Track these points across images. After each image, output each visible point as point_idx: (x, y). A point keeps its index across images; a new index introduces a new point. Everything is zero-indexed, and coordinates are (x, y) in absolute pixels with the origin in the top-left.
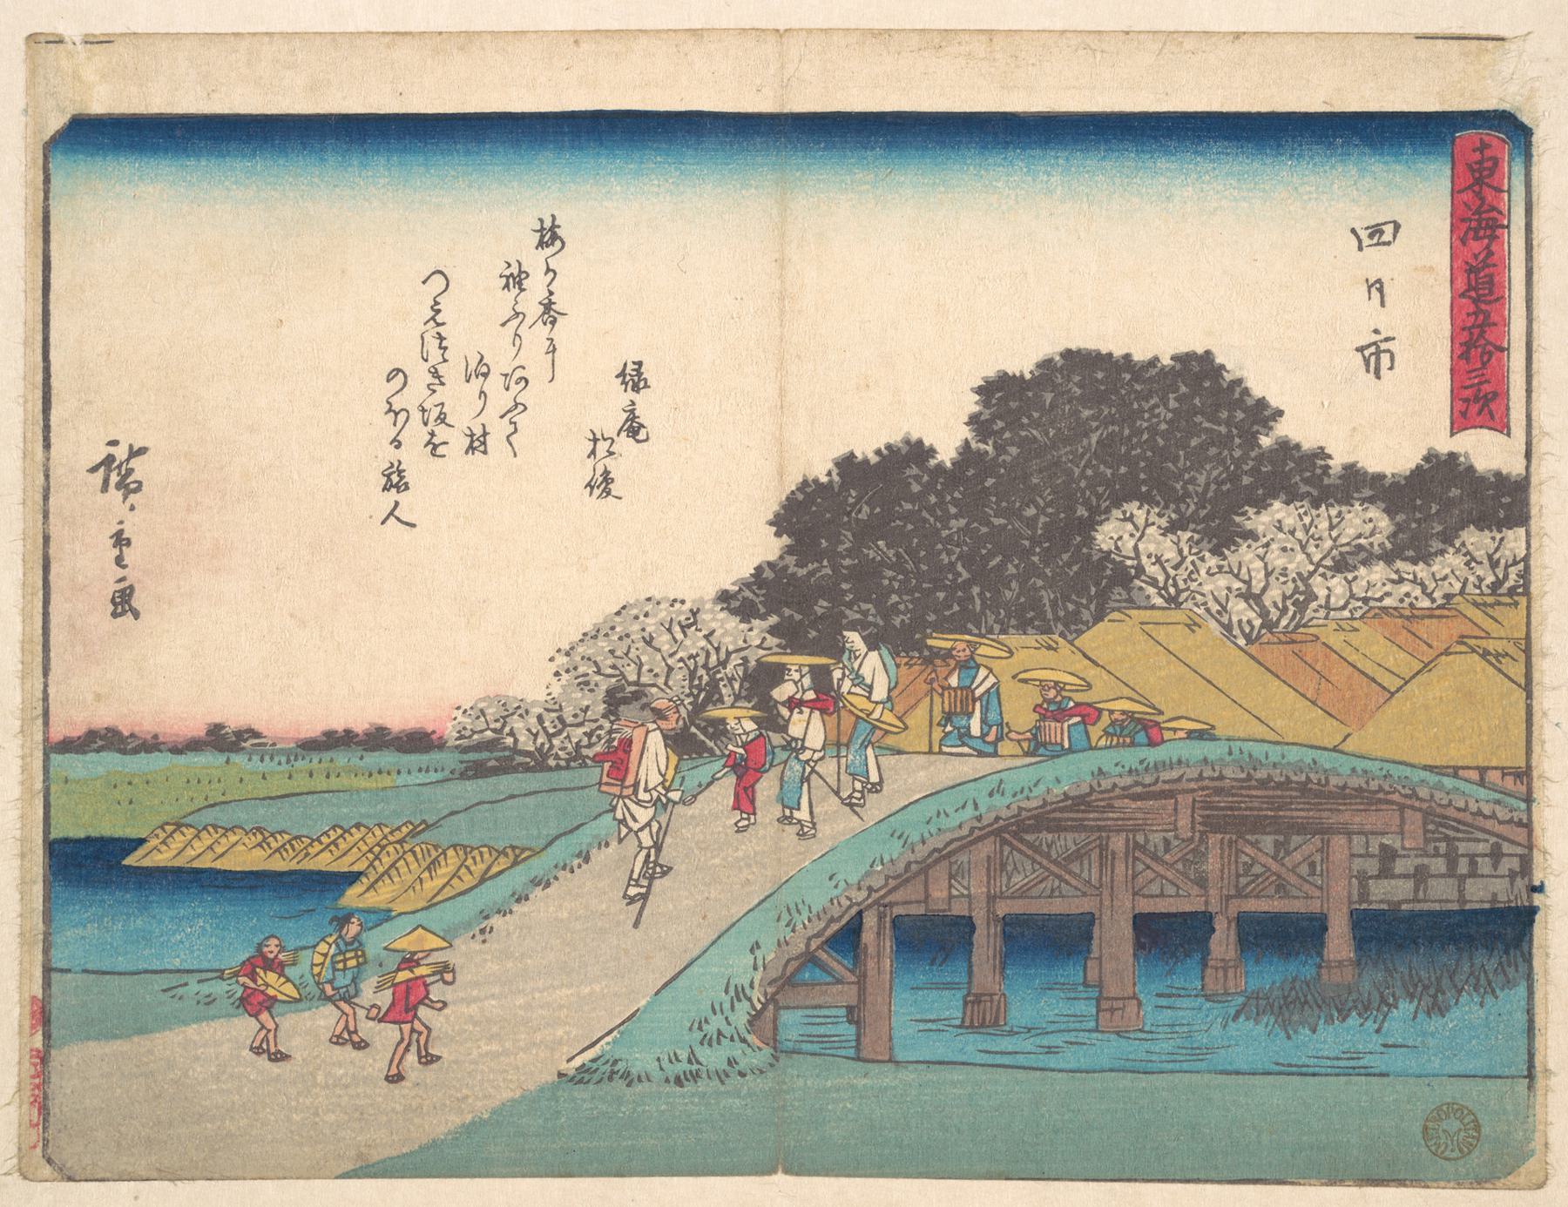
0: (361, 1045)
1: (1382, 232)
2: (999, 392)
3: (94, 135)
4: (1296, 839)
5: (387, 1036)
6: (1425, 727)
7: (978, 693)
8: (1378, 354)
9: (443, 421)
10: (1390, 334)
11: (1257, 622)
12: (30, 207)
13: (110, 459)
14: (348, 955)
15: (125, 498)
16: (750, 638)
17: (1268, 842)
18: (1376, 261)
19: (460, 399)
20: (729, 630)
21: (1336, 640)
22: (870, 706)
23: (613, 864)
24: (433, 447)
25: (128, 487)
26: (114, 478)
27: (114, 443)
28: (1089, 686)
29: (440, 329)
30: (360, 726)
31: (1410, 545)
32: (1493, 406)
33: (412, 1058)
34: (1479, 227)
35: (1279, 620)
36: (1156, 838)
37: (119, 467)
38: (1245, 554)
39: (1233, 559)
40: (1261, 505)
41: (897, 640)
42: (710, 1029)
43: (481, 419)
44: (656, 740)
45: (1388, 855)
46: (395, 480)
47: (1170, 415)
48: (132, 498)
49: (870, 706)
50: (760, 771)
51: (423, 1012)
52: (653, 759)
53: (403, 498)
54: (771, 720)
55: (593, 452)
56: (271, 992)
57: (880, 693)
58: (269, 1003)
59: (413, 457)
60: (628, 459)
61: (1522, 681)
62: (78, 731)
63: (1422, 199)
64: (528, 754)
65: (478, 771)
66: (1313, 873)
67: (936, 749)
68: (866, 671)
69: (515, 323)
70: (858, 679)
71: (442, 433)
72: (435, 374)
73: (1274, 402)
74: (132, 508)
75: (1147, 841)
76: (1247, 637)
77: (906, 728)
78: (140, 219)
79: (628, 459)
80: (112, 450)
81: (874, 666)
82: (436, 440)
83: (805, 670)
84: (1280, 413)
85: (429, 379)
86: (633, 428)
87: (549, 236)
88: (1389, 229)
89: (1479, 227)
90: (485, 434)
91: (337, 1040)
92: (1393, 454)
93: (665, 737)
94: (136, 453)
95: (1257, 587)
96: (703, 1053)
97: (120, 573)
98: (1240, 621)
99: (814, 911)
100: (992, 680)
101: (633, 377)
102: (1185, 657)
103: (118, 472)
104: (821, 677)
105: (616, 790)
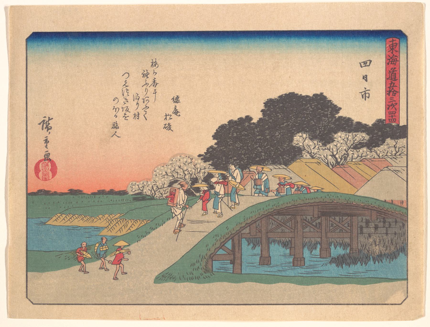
0: (107, 270)
1: (367, 63)
2: (269, 103)
3: (37, 37)
4: (345, 218)
5: (113, 268)
6: (377, 188)
7: (263, 180)
8: (365, 94)
9: (128, 111)
10: (369, 89)
11: (335, 162)
12: (387, 206)
13: (44, 121)
14: (104, 247)
15: (47, 131)
16: (206, 167)
17: (337, 218)
18: (364, 71)
19: (132, 105)
20: (201, 164)
21: (353, 167)
22: (236, 184)
23: (172, 224)
24: (125, 117)
25: (48, 128)
26: (45, 126)
27: (45, 117)
28: (291, 178)
29: (127, 87)
30: (108, 189)
31: (371, 144)
32: (396, 107)
33: (120, 272)
34: (392, 62)
35: (340, 161)
36: (309, 217)
37: (46, 123)
38: (331, 145)
39: (328, 146)
40: (336, 133)
41: (243, 167)
42: (196, 266)
43: (138, 110)
44: (182, 192)
45: (367, 222)
46: (115, 126)
47: (312, 109)
48: (49, 131)
49: (235, 184)
50: (209, 201)
51: (123, 262)
52: (181, 197)
53: (118, 130)
54: (212, 187)
55: (166, 118)
56: (84, 256)
57: (238, 180)
58: (84, 259)
59: (121, 121)
60: (175, 121)
61: (405, 179)
62: (36, 191)
63: (377, 53)
64: (149, 196)
65: (136, 199)
66: (348, 226)
67: (253, 194)
68: (235, 175)
69: (146, 86)
70: (233, 177)
71: (128, 114)
72: (126, 99)
73: (339, 106)
74: (50, 133)
75: (306, 217)
76: (332, 166)
77: (245, 189)
78: (54, 62)
79: (175, 121)
80: (45, 119)
81: (237, 173)
82: (126, 116)
83: (220, 174)
84: (340, 109)
85: (124, 100)
86: (176, 112)
87: (154, 64)
88: (368, 62)
89: (392, 62)
90: (139, 114)
91: (101, 268)
92: (369, 120)
93: (185, 192)
94: (49, 119)
95: (335, 153)
96: (194, 272)
97: (46, 150)
98: (330, 162)
99: (222, 235)
100: (266, 177)
101: (176, 100)
102: (314, 170)
103: (46, 124)
104: (224, 177)
105: (172, 205)
